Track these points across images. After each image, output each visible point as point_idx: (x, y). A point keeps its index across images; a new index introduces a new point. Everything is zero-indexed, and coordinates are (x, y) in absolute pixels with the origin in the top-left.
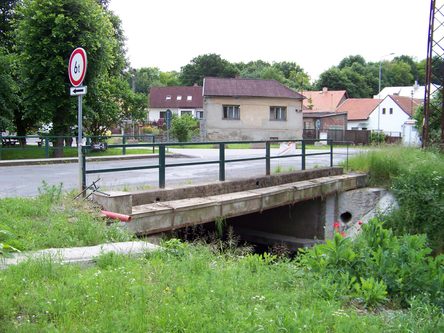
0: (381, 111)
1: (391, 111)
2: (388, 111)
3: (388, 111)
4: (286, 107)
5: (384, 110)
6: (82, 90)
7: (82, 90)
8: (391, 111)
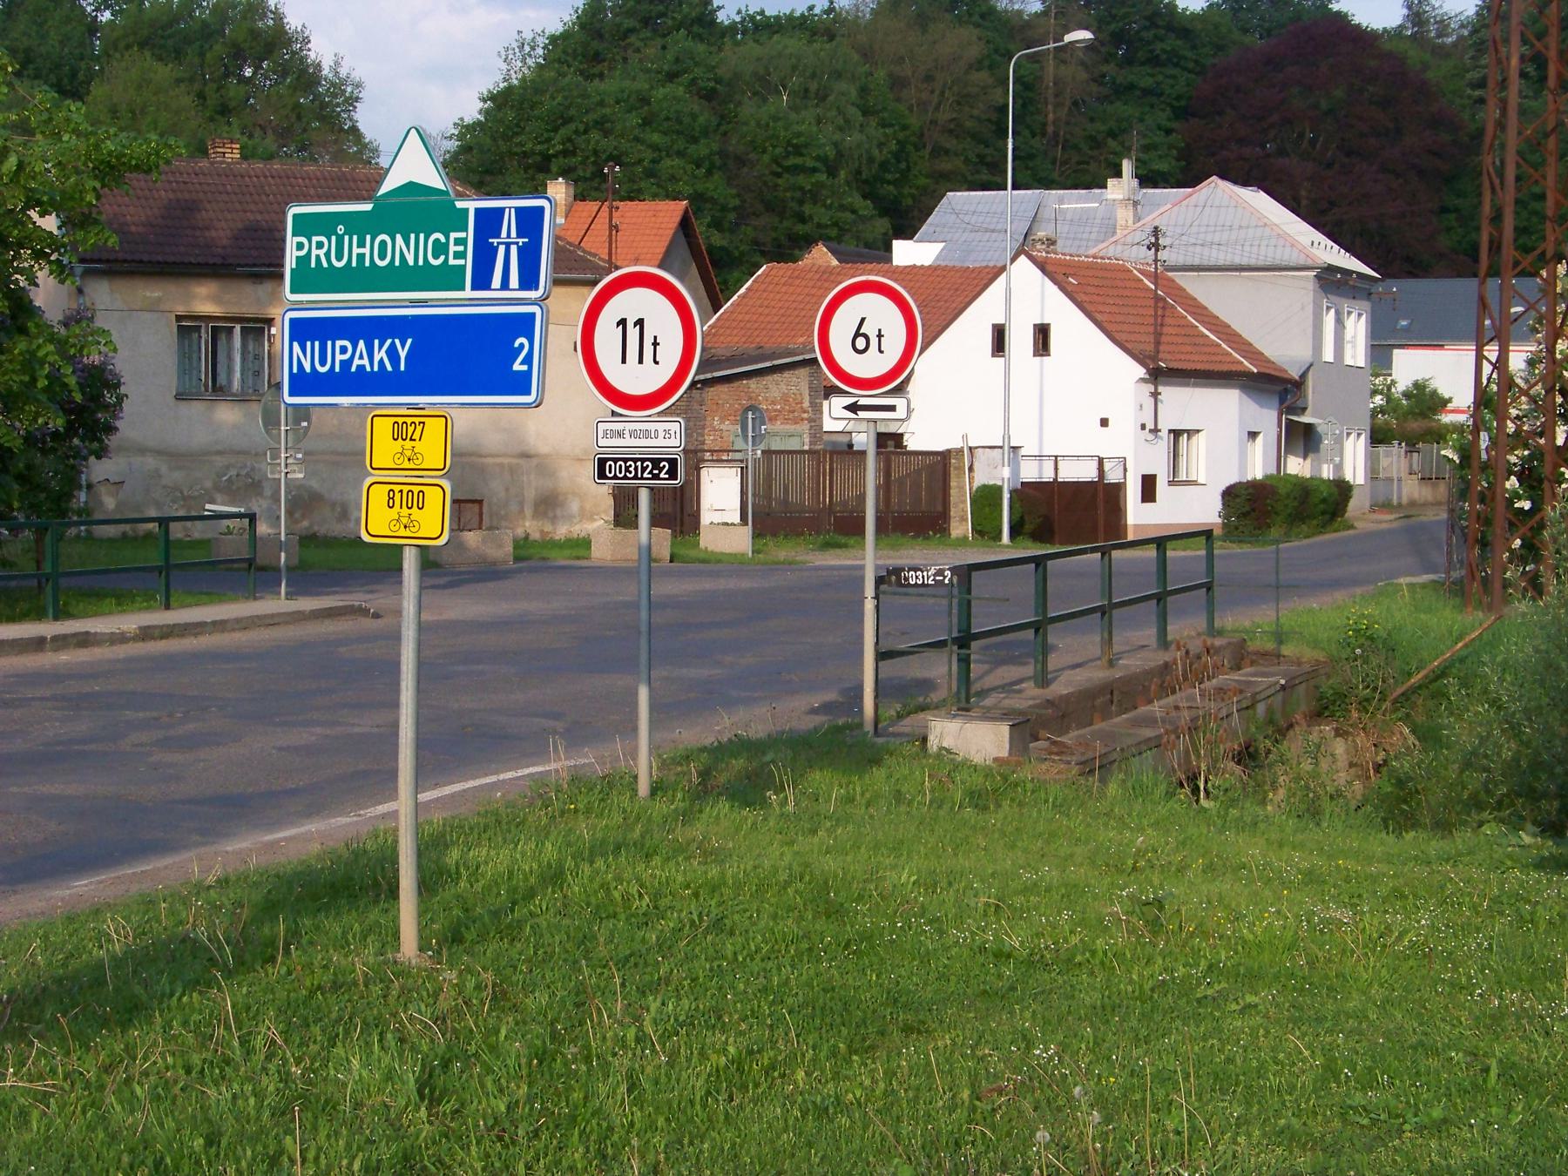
1: (1042, 336)
2: (1021, 340)
3: (1021, 340)
4: (180, 397)
6: (892, 408)
7: (892, 408)
8: (1042, 336)
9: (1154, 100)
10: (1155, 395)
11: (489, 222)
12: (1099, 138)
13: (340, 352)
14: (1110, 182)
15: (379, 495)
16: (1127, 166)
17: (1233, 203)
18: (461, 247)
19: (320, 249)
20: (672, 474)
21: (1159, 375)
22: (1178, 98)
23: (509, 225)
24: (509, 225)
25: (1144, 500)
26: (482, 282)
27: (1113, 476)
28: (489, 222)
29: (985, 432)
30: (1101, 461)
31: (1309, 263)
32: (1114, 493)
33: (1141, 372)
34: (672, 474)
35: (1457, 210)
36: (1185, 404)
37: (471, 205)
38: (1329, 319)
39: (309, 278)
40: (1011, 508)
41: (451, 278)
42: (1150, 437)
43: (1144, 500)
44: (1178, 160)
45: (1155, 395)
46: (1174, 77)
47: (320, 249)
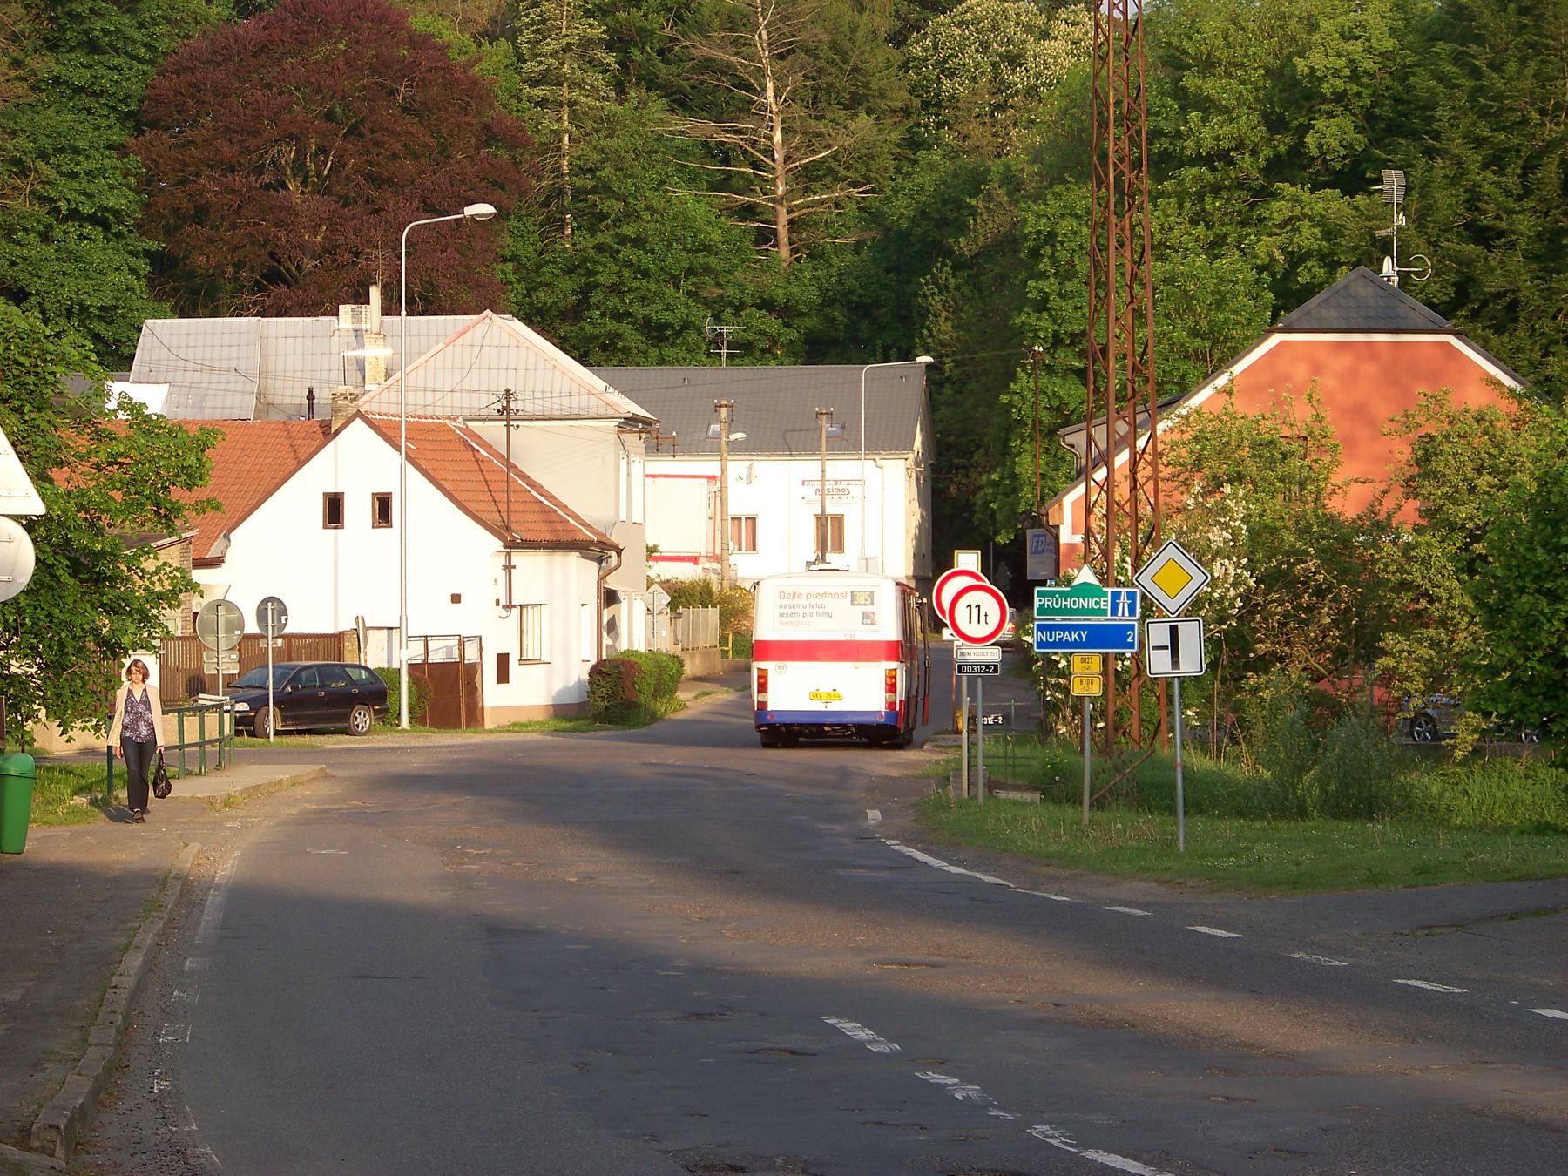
0: (318, 510)
1: (383, 508)
2: (358, 510)
3: (358, 510)
5: (334, 510)
8: (383, 508)
9: (90, 102)
10: (509, 568)
11: (1116, 596)
12: (27, 160)
13: (1057, 635)
14: (344, 309)
15: (1077, 680)
16: (375, 293)
17: (514, 343)
18: (1105, 602)
19: (1048, 602)
20: (996, 671)
21: (511, 545)
22: (126, 100)
23: (1124, 597)
24: (1124, 597)
25: (499, 682)
26: (1114, 612)
27: (471, 655)
28: (1116, 596)
29: (382, 613)
30: (462, 642)
31: (611, 412)
32: (473, 670)
33: (499, 544)
34: (996, 671)
35: (515, 258)
36: (538, 572)
37: (1109, 590)
38: (623, 463)
39: (1042, 610)
40: (410, 692)
41: (1104, 613)
42: (504, 613)
43: (499, 682)
44: (137, 191)
45: (509, 568)
46: (118, 69)
47: (1048, 602)
